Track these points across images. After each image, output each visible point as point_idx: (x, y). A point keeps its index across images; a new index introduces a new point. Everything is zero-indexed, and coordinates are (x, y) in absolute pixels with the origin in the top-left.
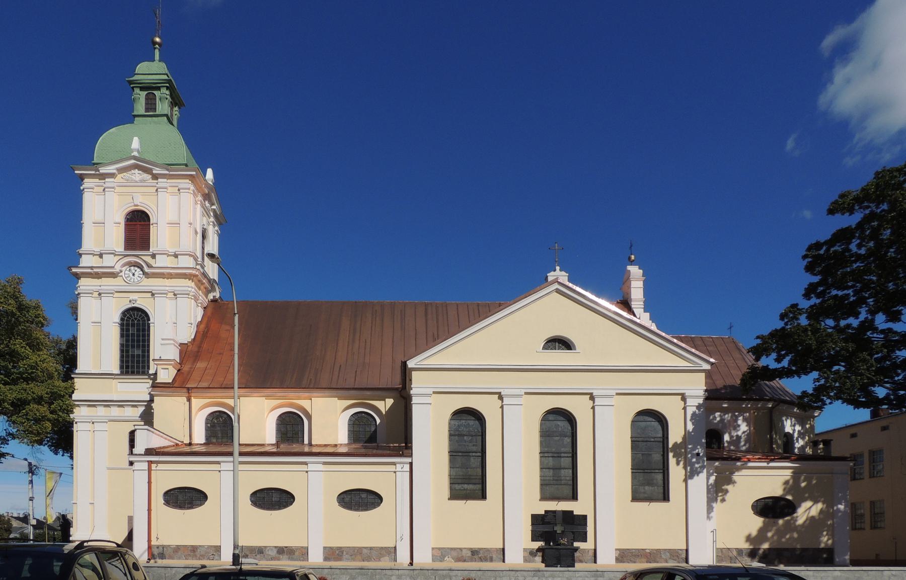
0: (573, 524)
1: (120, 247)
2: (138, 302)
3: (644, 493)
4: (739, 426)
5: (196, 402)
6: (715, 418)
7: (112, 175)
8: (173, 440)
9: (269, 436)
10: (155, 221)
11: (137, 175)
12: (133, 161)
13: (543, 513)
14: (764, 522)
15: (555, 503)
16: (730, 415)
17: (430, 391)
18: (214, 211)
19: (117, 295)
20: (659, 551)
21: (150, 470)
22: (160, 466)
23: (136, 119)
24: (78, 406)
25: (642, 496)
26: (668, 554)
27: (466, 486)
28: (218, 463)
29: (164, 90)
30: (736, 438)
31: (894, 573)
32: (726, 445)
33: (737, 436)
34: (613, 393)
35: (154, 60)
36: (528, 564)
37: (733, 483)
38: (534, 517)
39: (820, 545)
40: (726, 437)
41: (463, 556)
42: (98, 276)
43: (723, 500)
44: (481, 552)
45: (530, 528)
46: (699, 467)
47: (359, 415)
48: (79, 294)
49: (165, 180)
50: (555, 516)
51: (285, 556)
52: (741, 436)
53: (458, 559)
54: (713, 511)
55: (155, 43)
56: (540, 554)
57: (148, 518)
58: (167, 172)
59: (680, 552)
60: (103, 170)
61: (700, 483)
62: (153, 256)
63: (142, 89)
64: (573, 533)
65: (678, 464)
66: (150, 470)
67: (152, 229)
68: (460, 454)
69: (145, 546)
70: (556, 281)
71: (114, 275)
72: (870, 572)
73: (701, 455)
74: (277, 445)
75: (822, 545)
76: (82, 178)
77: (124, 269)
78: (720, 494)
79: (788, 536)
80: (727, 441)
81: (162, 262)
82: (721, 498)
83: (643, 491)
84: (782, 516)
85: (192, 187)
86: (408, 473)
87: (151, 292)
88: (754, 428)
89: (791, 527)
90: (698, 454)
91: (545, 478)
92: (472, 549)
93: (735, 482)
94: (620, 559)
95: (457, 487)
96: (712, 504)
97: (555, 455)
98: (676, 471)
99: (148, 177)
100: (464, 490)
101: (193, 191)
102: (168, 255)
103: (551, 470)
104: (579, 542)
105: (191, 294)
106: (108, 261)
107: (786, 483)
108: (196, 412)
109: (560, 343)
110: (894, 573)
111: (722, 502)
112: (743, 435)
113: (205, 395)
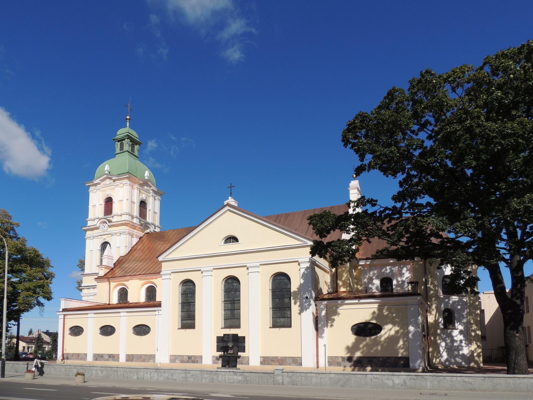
0: (238, 342)
3: (280, 322)
4: (404, 274)
5: (113, 284)
6: (386, 270)
7: (98, 184)
8: (94, 303)
9: (142, 299)
11: (108, 181)
12: (105, 176)
13: (223, 336)
14: (356, 339)
15: (229, 330)
16: (397, 267)
17: (211, 268)
18: (153, 190)
19: (99, 237)
20: (285, 358)
21: (64, 319)
22: (69, 317)
23: (117, 155)
24: (83, 289)
25: (279, 324)
26: (291, 360)
27: (188, 321)
28: (119, 313)
29: (126, 140)
30: (402, 282)
31: (375, 376)
32: (394, 287)
33: (402, 281)
34: (258, 264)
35: (126, 127)
36: (264, 366)
37: (338, 314)
38: (218, 338)
39: (398, 354)
40: (395, 282)
41: (184, 360)
43: (332, 326)
44: (193, 358)
45: (216, 344)
46: (307, 305)
47: (122, 289)
49: (118, 181)
50: (229, 337)
51: (111, 359)
52: (405, 281)
53: (182, 362)
54: (324, 333)
55: (127, 119)
56: (221, 359)
58: (117, 178)
59: (298, 358)
61: (308, 315)
62: (113, 217)
63: (118, 141)
64: (238, 347)
65: (295, 303)
66: (64, 319)
68: (186, 304)
69: (61, 354)
70: (228, 205)
71: (97, 228)
72: (356, 376)
73: (308, 297)
74: (119, 303)
75: (400, 355)
76: (89, 186)
77: (101, 225)
78: (330, 322)
79: (375, 349)
80: (395, 285)
82: (330, 324)
83: (279, 321)
84: (370, 335)
85: (128, 182)
86: (63, 319)
88: (413, 275)
89: (377, 342)
90: (307, 298)
91: (227, 316)
92: (188, 356)
93: (339, 314)
94: (264, 362)
95: (185, 322)
96: (324, 328)
97: (232, 302)
98: (295, 308)
99: (112, 181)
100: (188, 323)
101: (129, 184)
102: (118, 216)
103: (230, 311)
104: (241, 352)
105: (126, 232)
107: (374, 313)
108: (114, 287)
109: (232, 239)
110: (375, 376)
111: (331, 327)
112: (407, 280)
113: (114, 280)
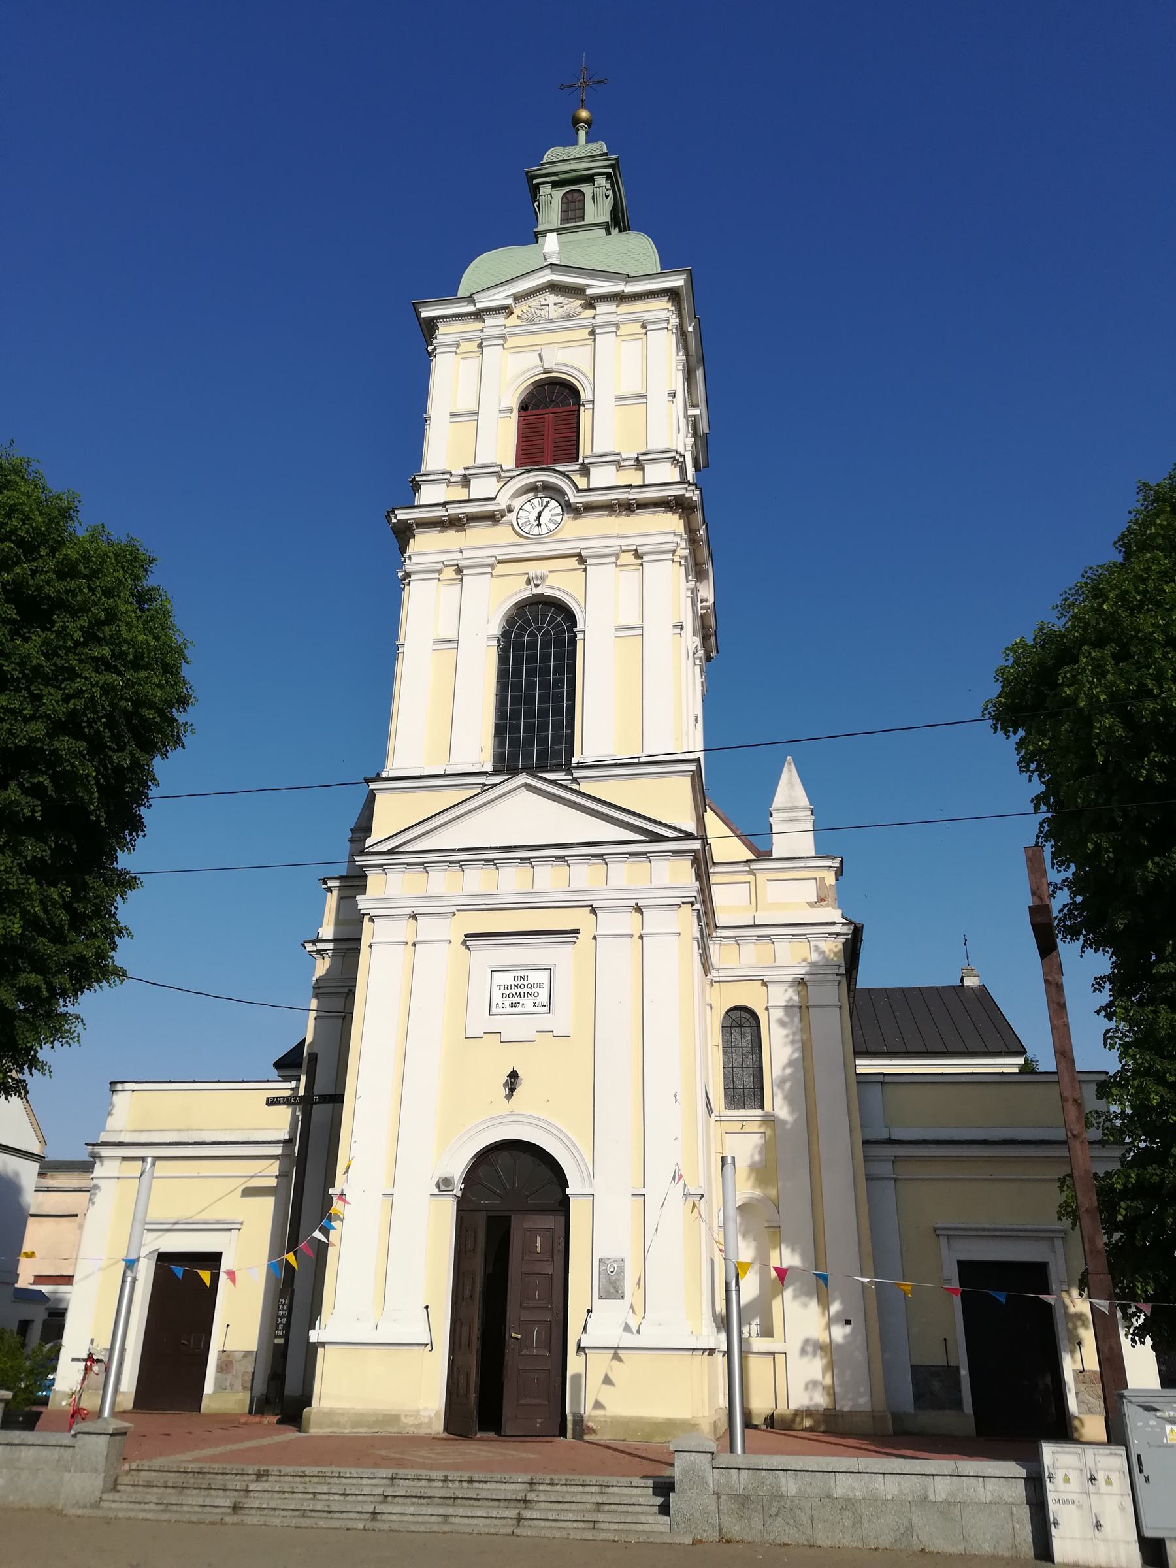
1: (507, 456)
2: (548, 582)
10: (589, 397)
42: (455, 523)
48: (408, 575)
55: (576, 121)
57: (566, 1222)
60: (483, 302)
63: (555, 185)
67: (585, 416)
71: (493, 518)
77: (517, 503)
81: (602, 476)
87: (579, 555)
99: (575, 304)
106: (482, 487)
